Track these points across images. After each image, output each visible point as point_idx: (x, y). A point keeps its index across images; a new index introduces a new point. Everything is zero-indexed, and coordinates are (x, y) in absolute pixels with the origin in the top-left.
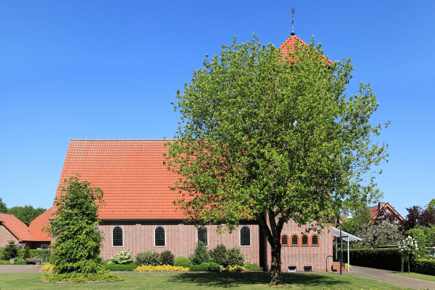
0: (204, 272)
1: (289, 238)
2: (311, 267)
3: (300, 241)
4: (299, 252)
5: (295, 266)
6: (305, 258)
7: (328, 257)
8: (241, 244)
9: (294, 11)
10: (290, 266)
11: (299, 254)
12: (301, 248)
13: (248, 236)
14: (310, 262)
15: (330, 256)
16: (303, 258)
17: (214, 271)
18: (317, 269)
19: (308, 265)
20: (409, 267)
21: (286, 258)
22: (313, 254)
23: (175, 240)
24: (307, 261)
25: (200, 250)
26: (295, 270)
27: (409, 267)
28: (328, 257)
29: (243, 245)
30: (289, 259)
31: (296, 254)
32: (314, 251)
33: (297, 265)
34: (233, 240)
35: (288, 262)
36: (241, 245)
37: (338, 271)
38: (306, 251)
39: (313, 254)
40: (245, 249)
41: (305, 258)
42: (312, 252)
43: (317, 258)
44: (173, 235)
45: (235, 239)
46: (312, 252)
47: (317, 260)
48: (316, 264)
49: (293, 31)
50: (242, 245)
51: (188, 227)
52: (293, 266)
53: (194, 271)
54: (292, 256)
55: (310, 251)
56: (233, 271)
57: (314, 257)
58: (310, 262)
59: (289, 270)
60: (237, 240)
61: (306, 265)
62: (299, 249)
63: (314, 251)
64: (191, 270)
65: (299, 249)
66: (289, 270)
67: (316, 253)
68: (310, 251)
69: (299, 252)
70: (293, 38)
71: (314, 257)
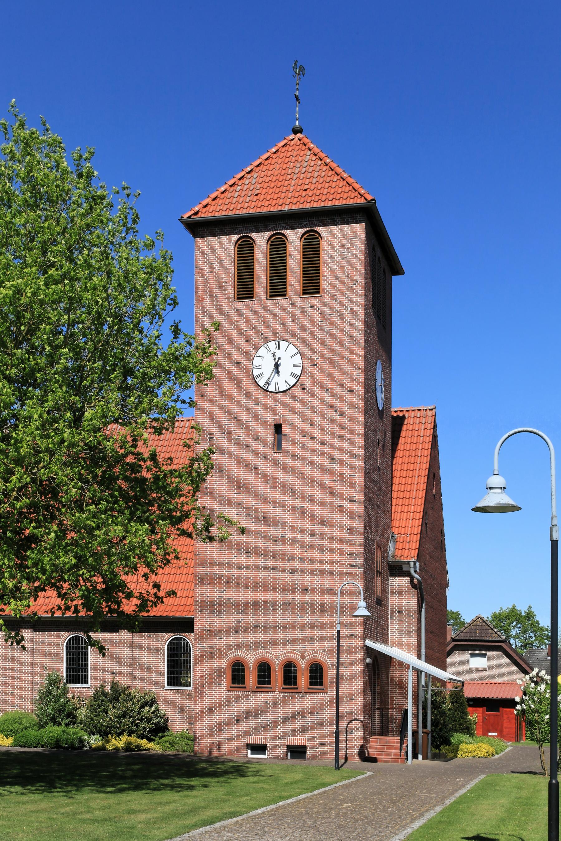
0: (39, 749)
1: (249, 668)
2: (305, 747)
3: (277, 678)
4: (275, 706)
5: (264, 742)
6: (289, 723)
7: (351, 721)
8: (168, 683)
9: (302, 69)
10: (251, 741)
11: (275, 713)
12: (279, 696)
13: (187, 663)
14: (303, 733)
15: (355, 720)
16: (285, 722)
17: (67, 748)
18: (322, 752)
19: (298, 741)
20: (304, 796)
21: (243, 722)
22: (312, 713)
23: (13, 668)
24: (294, 731)
25: (362, 722)
26: (265, 754)
27: (304, 796)
28: (351, 721)
29: (174, 686)
30: (247, 725)
31: (266, 712)
32: (312, 704)
33: (268, 740)
34: (149, 673)
35: (247, 733)
36: (168, 685)
37: (380, 761)
38: (294, 704)
39: (312, 713)
40: (178, 695)
41: (289, 723)
42: (308, 709)
43: (321, 724)
44: (9, 656)
45: (153, 669)
46: (308, 709)
47: (322, 730)
48: (317, 739)
49: (297, 122)
50: (171, 685)
51: (42, 638)
52: (259, 742)
53: (21, 747)
54: (257, 717)
55: (302, 704)
56: (117, 750)
57: (312, 721)
58: (303, 733)
59: (252, 754)
60: (157, 671)
61: (292, 743)
62: (275, 698)
63: (312, 704)
64: (16, 744)
65: (275, 698)
66: (252, 754)
67: (317, 709)
68: (302, 704)
69: (275, 706)
70: (296, 139)
71: (312, 721)
